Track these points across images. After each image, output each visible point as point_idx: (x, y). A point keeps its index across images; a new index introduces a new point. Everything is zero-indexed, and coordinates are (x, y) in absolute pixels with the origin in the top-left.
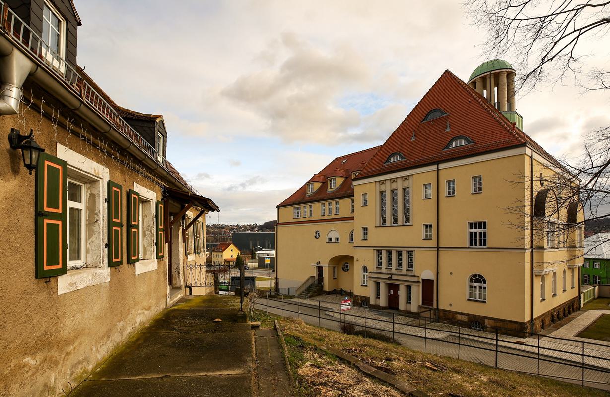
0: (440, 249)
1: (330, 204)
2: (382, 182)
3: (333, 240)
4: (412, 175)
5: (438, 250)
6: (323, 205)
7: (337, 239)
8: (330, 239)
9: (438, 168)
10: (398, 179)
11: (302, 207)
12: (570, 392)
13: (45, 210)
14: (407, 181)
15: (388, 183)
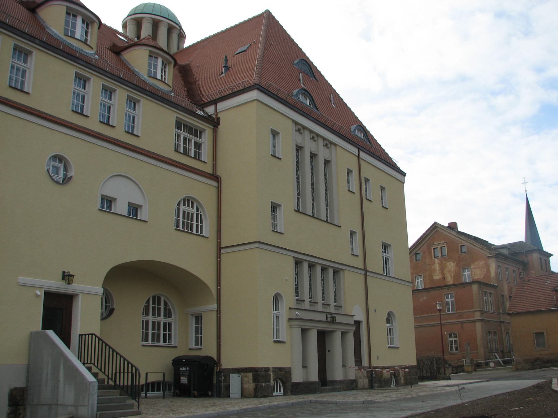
3: (121, 207)
5: (366, 275)
6: (82, 80)
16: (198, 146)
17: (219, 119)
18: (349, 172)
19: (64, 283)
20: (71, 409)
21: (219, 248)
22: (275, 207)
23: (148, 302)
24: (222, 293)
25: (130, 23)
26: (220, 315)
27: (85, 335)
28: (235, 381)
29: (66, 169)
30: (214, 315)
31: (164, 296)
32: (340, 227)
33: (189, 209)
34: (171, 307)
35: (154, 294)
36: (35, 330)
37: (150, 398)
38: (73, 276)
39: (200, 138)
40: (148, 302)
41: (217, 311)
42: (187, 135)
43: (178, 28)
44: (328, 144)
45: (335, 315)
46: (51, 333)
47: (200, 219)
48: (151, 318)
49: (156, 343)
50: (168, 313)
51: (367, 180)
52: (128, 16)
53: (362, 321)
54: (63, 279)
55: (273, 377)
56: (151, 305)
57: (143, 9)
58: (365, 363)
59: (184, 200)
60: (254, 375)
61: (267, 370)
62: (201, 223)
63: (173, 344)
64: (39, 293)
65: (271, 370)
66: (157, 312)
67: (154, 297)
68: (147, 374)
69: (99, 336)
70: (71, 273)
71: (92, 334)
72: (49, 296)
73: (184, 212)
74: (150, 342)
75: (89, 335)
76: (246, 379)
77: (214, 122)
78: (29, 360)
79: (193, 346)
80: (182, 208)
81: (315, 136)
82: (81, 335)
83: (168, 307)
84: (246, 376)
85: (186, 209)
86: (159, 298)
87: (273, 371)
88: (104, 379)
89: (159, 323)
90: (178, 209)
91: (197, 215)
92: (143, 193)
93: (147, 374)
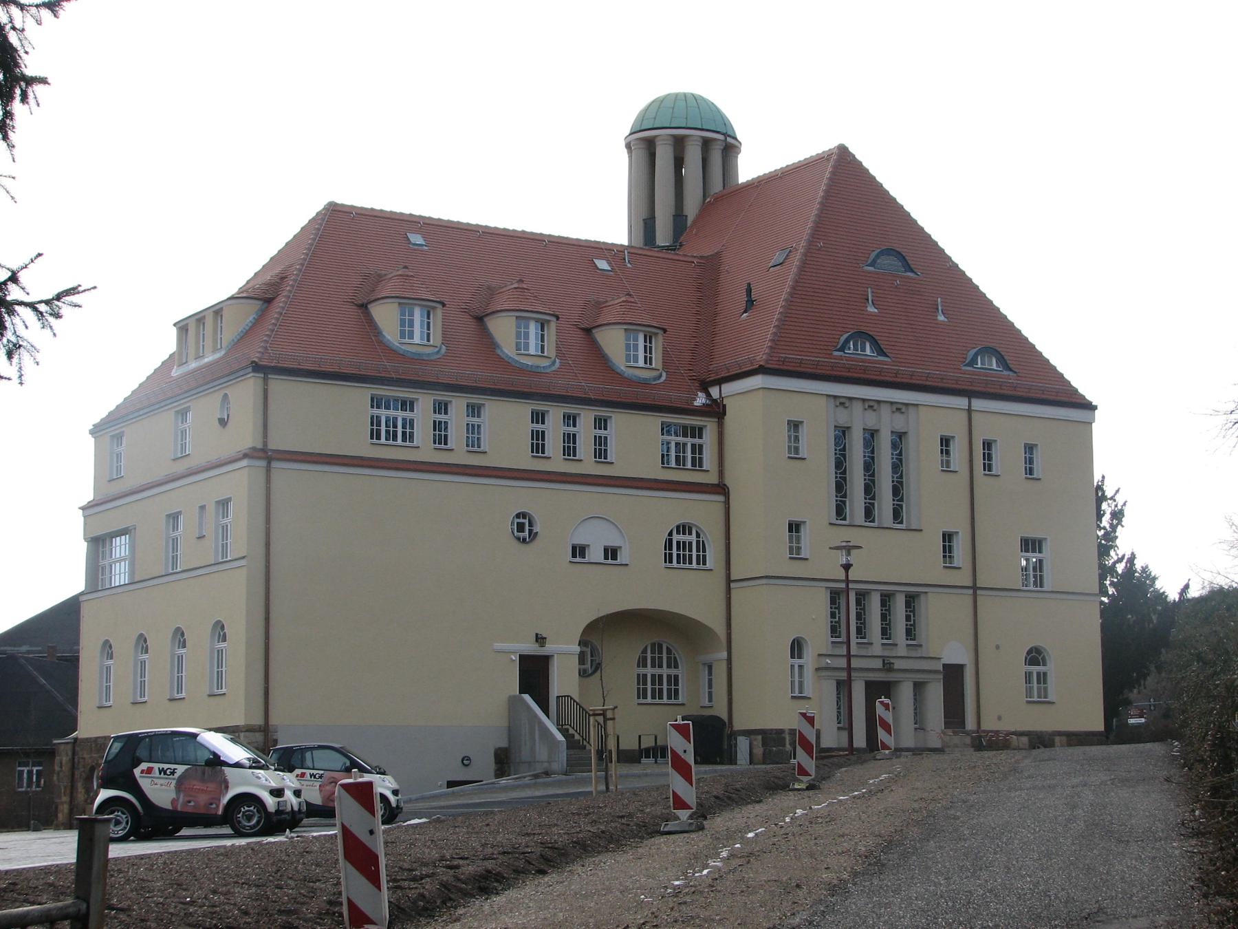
0: (979, 592)
1: (571, 419)
2: (843, 402)
3: (596, 554)
4: (917, 405)
5: (975, 596)
6: (539, 417)
7: (611, 553)
8: (579, 551)
9: (970, 405)
10: (882, 405)
11: (424, 403)
12: (1147, 797)
13: (135, 770)
14: (874, 413)
15: (858, 408)
16: (697, 449)
17: (724, 406)
18: (945, 442)
19: (537, 645)
20: (546, 765)
21: (729, 581)
22: (794, 527)
23: (645, 651)
24: (733, 637)
25: (636, 147)
26: (731, 664)
27: (562, 696)
28: (743, 744)
29: (531, 524)
30: (724, 665)
31: (666, 642)
32: (921, 530)
33: (686, 538)
34: (677, 655)
35: (656, 640)
36: (512, 694)
37: (660, 764)
38: (545, 638)
39: (700, 437)
40: (645, 651)
41: (727, 660)
42: (681, 439)
43: (721, 137)
44: (899, 408)
45: (892, 661)
46: (527, 697)
47: (701, 547)
48: (649, 671)
49: (657, 701)
50: (673, 663)
51: (988, 445)
52: (630, 135)
53: (965, 665)
54: (537, 641)
55: (789, 740)
56: (649, 655)
57: (655, 118)
58: (970, 724)
59: (678, 527)
60: (763, 739)
61: (780, 732)
62: (704, 551)
63: (680, 700)
64: (514, 658)
65: (787, 732)
66: (657, 663)
67: (653, 645)
68: (640, 736)
69: (577, 701)
70: (544, 636)
71: (568, 696)
72: (524, 659)
73: (678, 543)
74: (649, 700)
75: (565, 696)
76: (755, 743)
77: (717, 410)
78: (509, 722)
79: (707, 703)
80: (676, 538)
81: (871, 405)
82: (558, 697)
83: (672, 656)
84: (755, 740)
85: (681, 537)
86: (660, 646)
87: (789, 734)
88: (580, 740)
89: (661, 676)
90: (671, 541)
91: (698, 542)
92: (621, 532)
93: (640, 736)
